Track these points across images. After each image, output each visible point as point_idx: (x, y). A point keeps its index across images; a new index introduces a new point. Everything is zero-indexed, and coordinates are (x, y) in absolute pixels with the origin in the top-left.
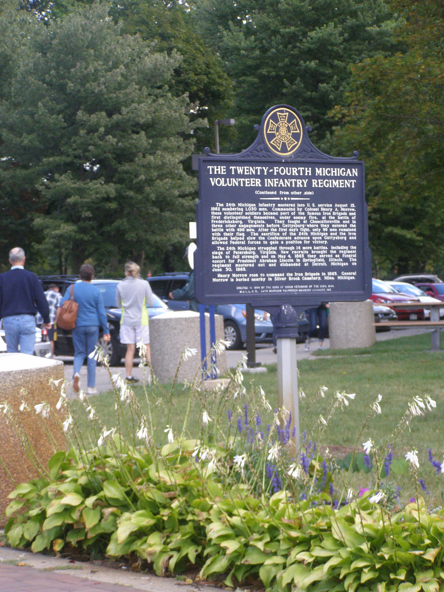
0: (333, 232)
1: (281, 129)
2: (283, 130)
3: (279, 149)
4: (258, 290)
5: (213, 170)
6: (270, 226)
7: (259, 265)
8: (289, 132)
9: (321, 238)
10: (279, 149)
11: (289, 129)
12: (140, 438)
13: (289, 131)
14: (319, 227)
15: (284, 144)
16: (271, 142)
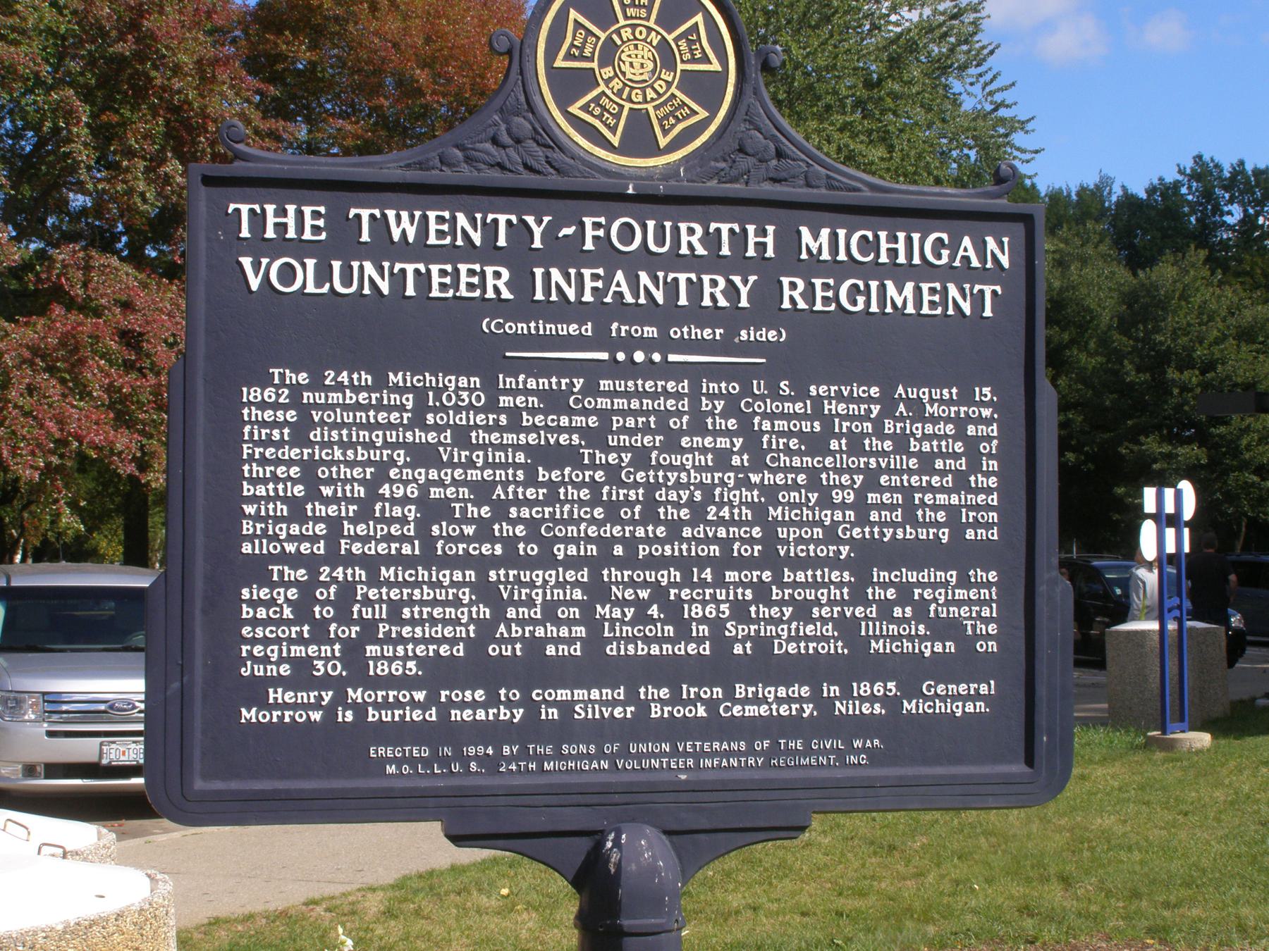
1: (626, 53)
2: (637, 61)
4: (482, 760)
11: (666, 55)
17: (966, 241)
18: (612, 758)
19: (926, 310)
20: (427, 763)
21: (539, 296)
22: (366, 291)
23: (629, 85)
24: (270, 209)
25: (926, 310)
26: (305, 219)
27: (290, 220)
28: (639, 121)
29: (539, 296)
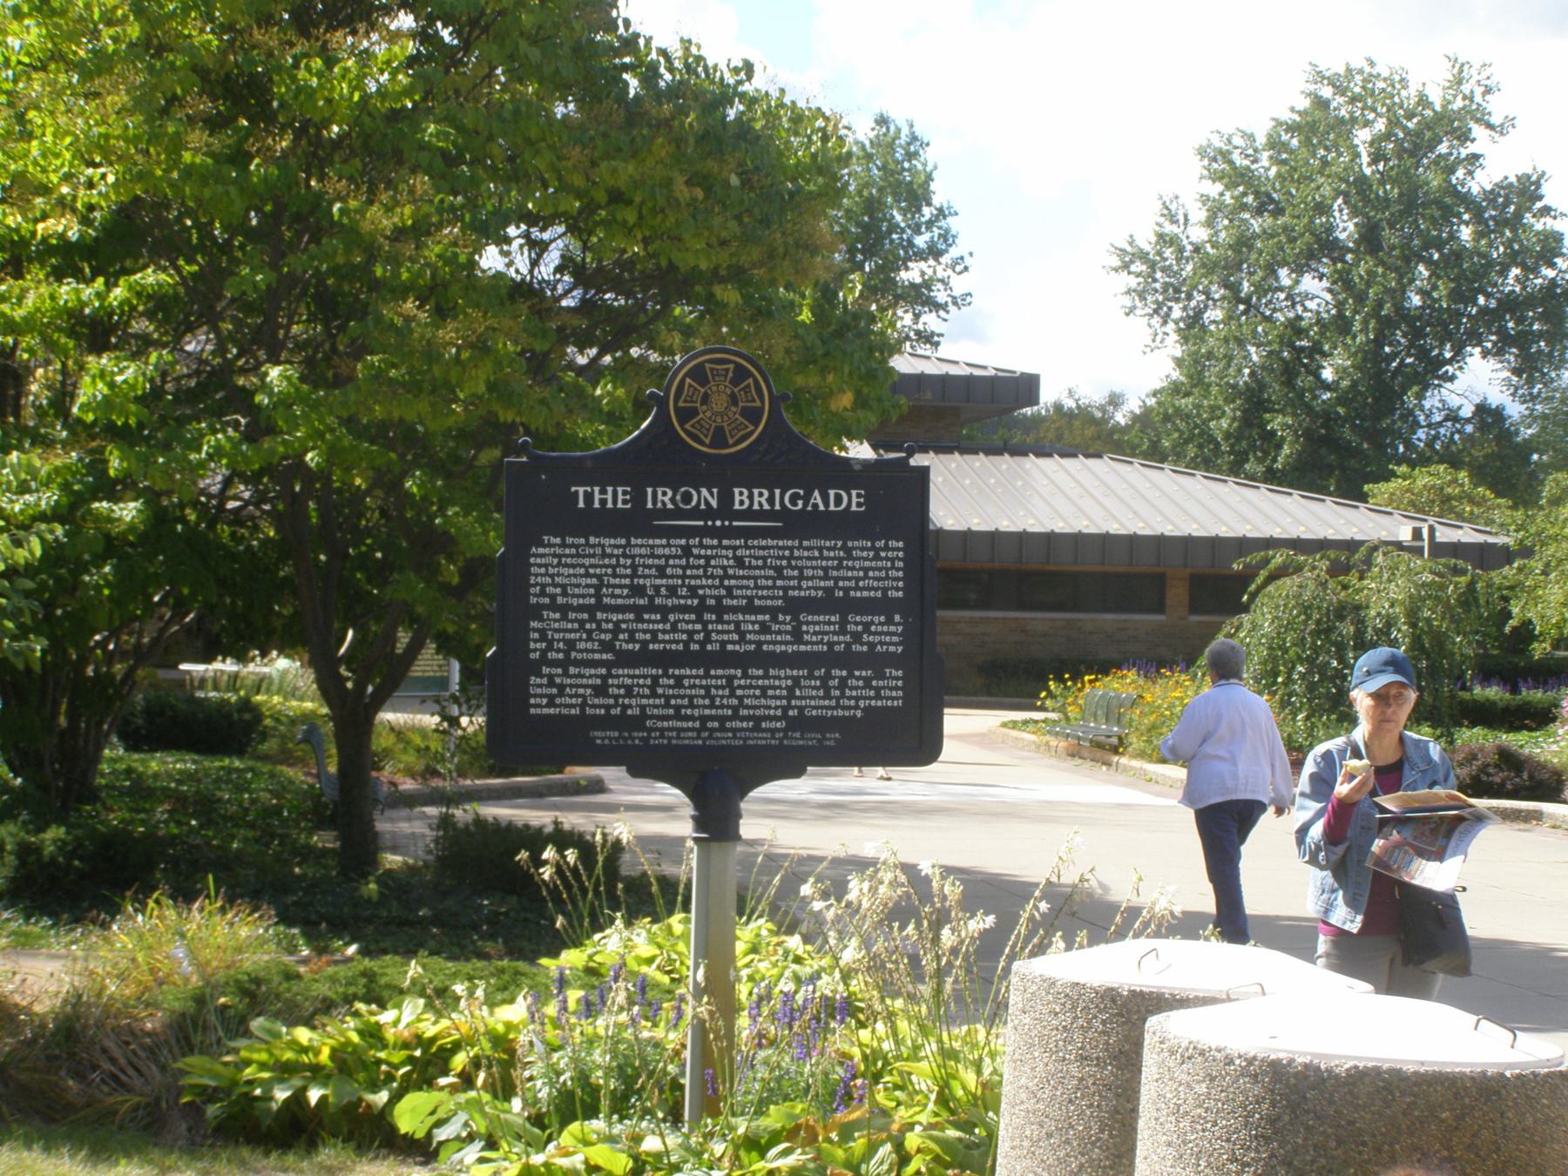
0: (780, 698)
1: (714, 398)
2: (719, 402)
3: (707, 441)
4: (641, 739)
5: (589, 497)
6: (630, 646)
7: (709, 647)
8: (735, 403)
9: (770, 692)
10: (707, 441)
11: (734, 399)
12: (403, 1131)
13: (735, 403)
14: (708, 695)
15: (719, 430)
16: (731, 366)
17: (816, 493)
18: (704, 739)
19: (620, 505)
20: (617, 739)
21: (650, 505)
22: (703, 507)
23: (716, 414)
24: (597, 489)
25: (620, 505)
26: (892, 594)
27: (609, 497)
28: (719, 431)
29: (650, 505)
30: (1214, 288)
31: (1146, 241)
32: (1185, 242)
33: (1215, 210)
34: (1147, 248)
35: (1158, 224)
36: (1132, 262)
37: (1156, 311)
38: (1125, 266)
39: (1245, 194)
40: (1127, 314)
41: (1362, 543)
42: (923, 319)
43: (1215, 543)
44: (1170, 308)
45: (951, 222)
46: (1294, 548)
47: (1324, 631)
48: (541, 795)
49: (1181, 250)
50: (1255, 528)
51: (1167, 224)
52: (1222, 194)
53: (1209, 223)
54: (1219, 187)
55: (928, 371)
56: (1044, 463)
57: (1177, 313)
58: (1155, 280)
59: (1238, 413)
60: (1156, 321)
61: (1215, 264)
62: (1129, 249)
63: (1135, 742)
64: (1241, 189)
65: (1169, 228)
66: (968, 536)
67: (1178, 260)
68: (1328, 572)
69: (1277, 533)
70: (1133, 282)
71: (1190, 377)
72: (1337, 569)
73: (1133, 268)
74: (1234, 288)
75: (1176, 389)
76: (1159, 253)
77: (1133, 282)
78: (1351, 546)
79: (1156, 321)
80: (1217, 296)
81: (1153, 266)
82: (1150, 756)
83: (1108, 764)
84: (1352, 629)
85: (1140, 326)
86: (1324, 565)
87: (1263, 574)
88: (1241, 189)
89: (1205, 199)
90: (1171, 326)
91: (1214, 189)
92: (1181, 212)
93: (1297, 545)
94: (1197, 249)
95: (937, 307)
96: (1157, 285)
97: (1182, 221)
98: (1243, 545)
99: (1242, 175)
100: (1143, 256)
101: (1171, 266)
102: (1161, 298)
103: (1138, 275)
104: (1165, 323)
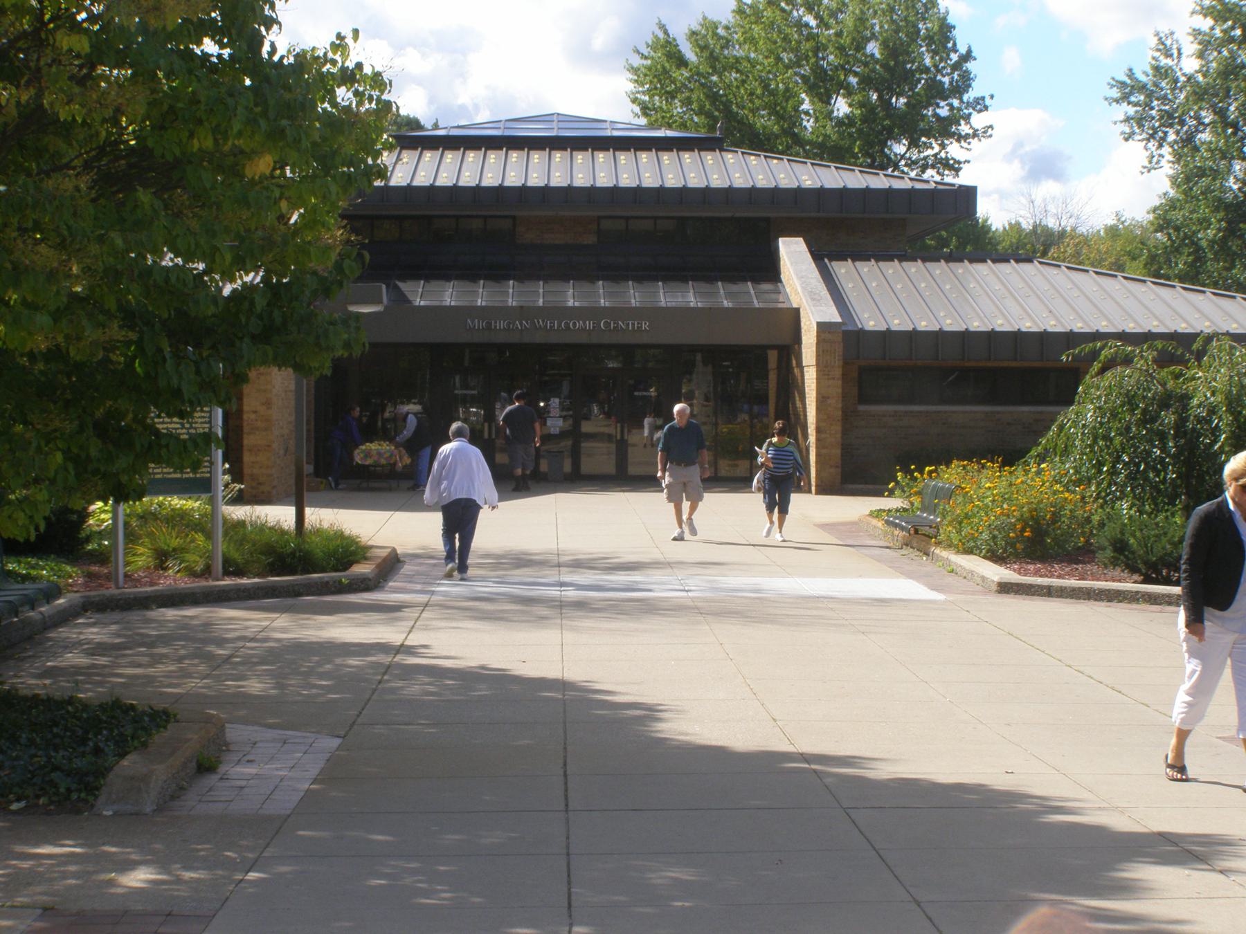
30: (1203, 113)
31: (1143, 74)
32: (1179, 74)
33: (1206, 44)
34: (1143, 78)
35: (1154, 58)
36: (1131, 93)
37: (1152, 136)
38: (1125, 98)
39: (1233, 28)
40: (1126, 140)
41: (1197, 335)
42: (949, 149)
43: (1044, 338)
44: (1166, 133)
45: (970, 66)
46: (1120, 340)
47: (1148, 418)
48: (298, 594)
49: (1176, 81)
50: (1192, 326)
51: (1162, 58)
52: (1212, 29)
53: (1201, 55)
54: (1210, 22)
55: (873, 186)
56: (1025, 268)
57: (1172, 137)
58: (1152, 108)
59: (1223, 224)
60: (1152, 145)
61: (1206, 92)
62: (1129, 81)
63: (948, 531)
64: (1230, 23)
65: (1164, 61)
66: (887, 336)
67: (1173, 90)
68: (1155, 361)
69: (1104, 327)
70: (1131, 110)
71: (1185, 193)
72: (1164, 360)
73: (1133, 99)
74: (1221, 114)
75: (1172, 205)
76: (1156, 85)
77: (1131, 110)
78: (1184, 339)
79: (1152, 145)
80: (1207, 121)
81: (1150, 95)
82: (956, 547)
83: (927, 554)
84: (1173, 418)
85: (1137, 151)
86: (1150, 355)
87: (1096, 366)
88: (1230, 23)
89: (1196, 33)
90: (1166, 150)
91: (1206, 24)
92: (1175, 46)
93: (1123, 337)
94: (1190, 78)
95: (960, 138)
96: (1153, 112)
97: (1175, 55)
98: (1071, 339)
99: (1230, 11)
100: (1142, 88)
101: (1166, 95)
102: (1157, 124)
103: (1136, 104)
104: (1160, 146)
